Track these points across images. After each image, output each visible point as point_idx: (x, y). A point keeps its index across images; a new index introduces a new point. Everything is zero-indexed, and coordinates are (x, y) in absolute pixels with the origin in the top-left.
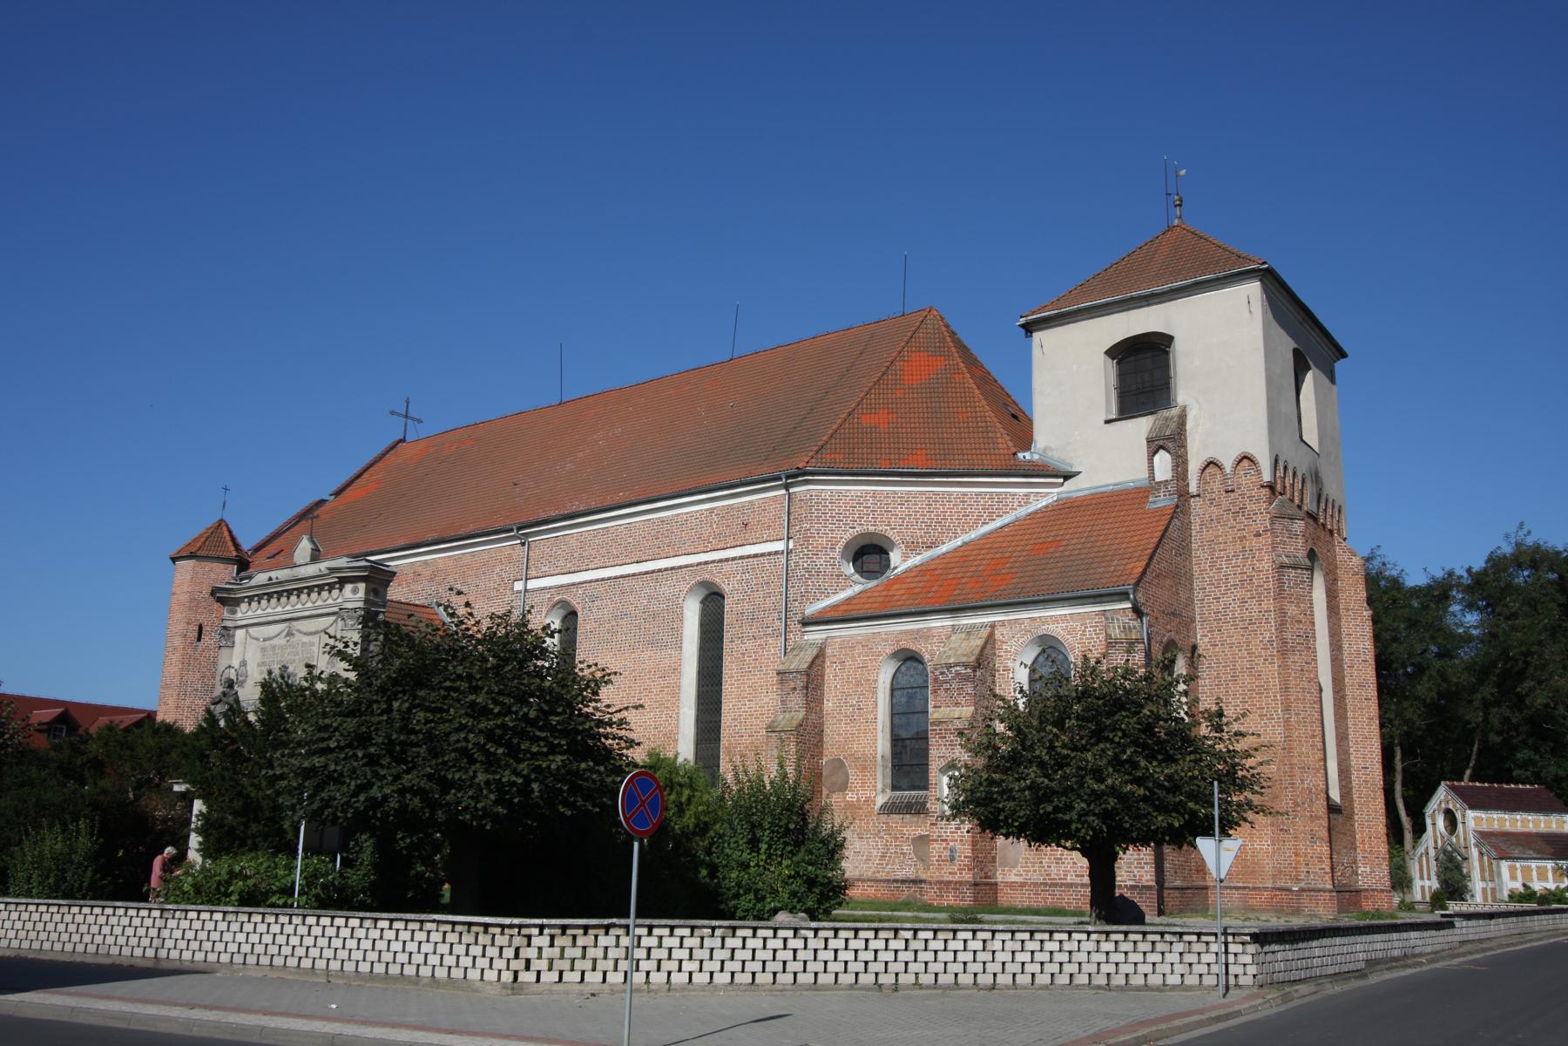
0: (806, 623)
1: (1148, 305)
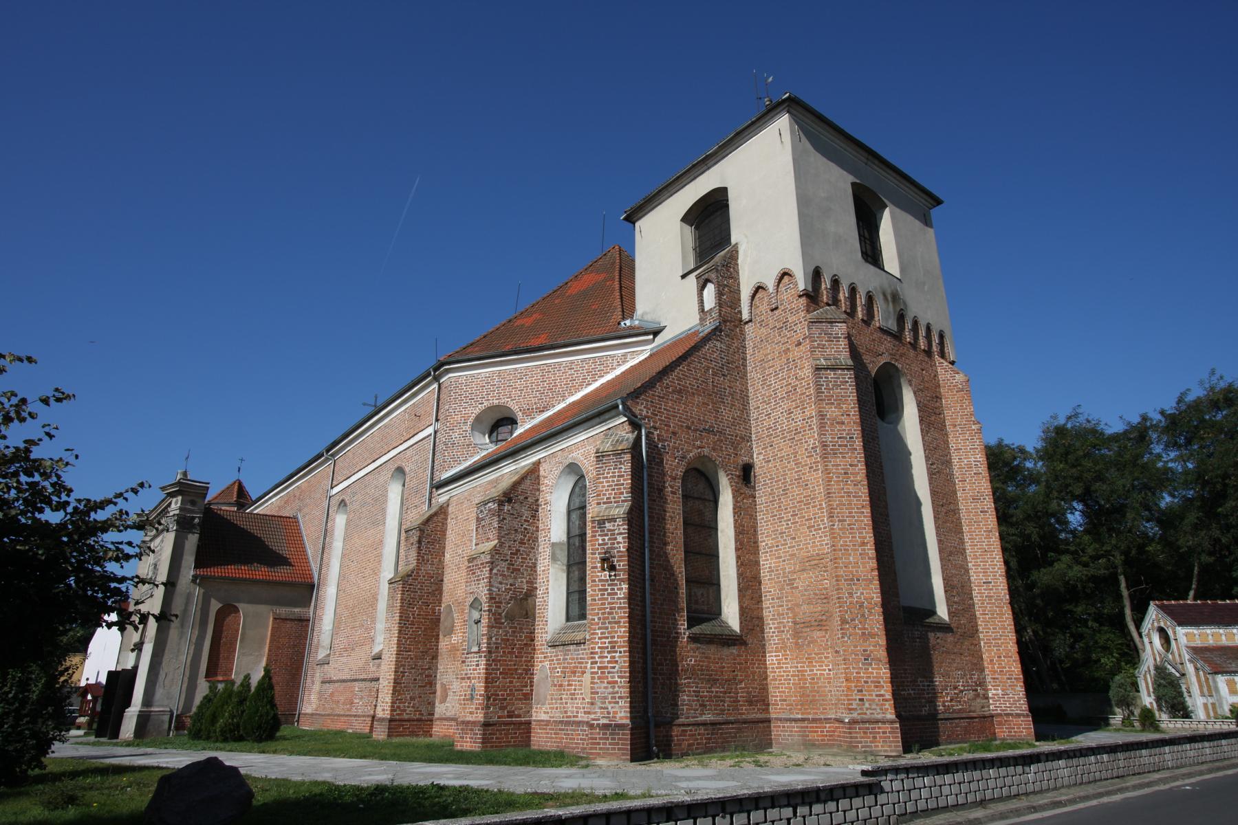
1: (709, 168)
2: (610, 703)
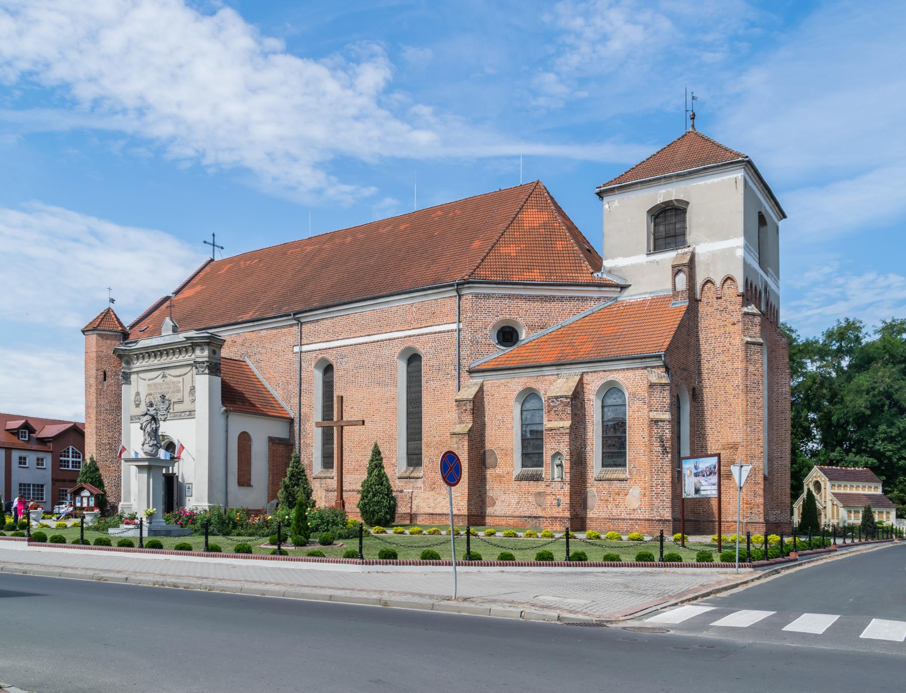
0: (471, 372)
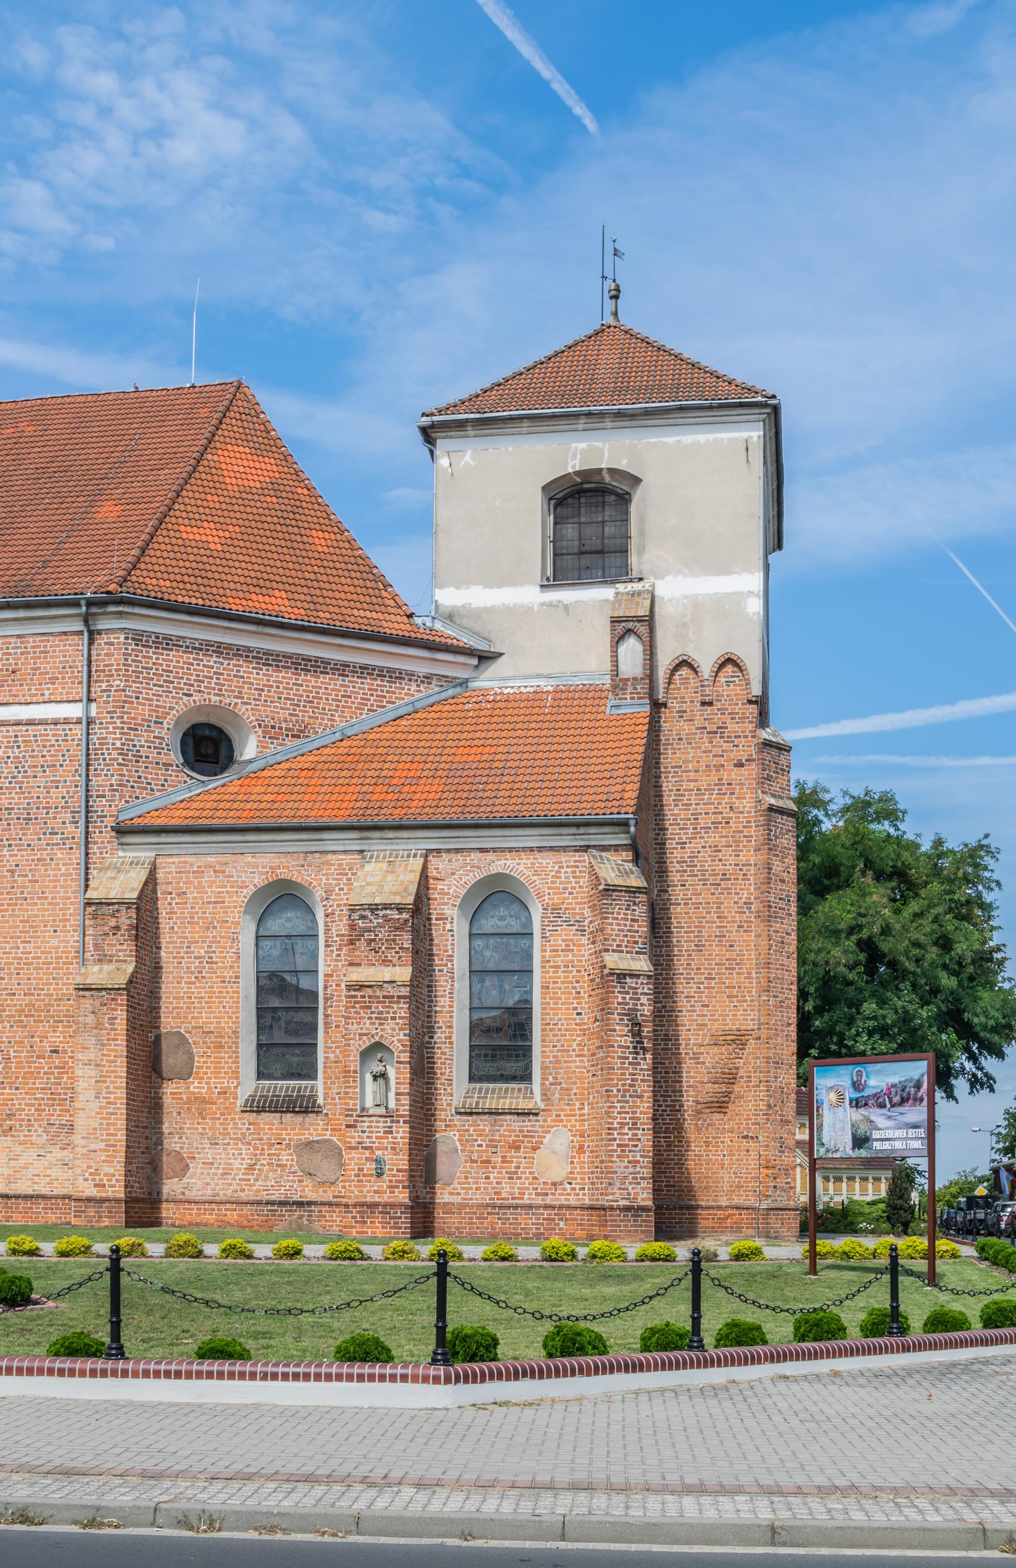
0: (122, 831)
2: (631, 1183)
